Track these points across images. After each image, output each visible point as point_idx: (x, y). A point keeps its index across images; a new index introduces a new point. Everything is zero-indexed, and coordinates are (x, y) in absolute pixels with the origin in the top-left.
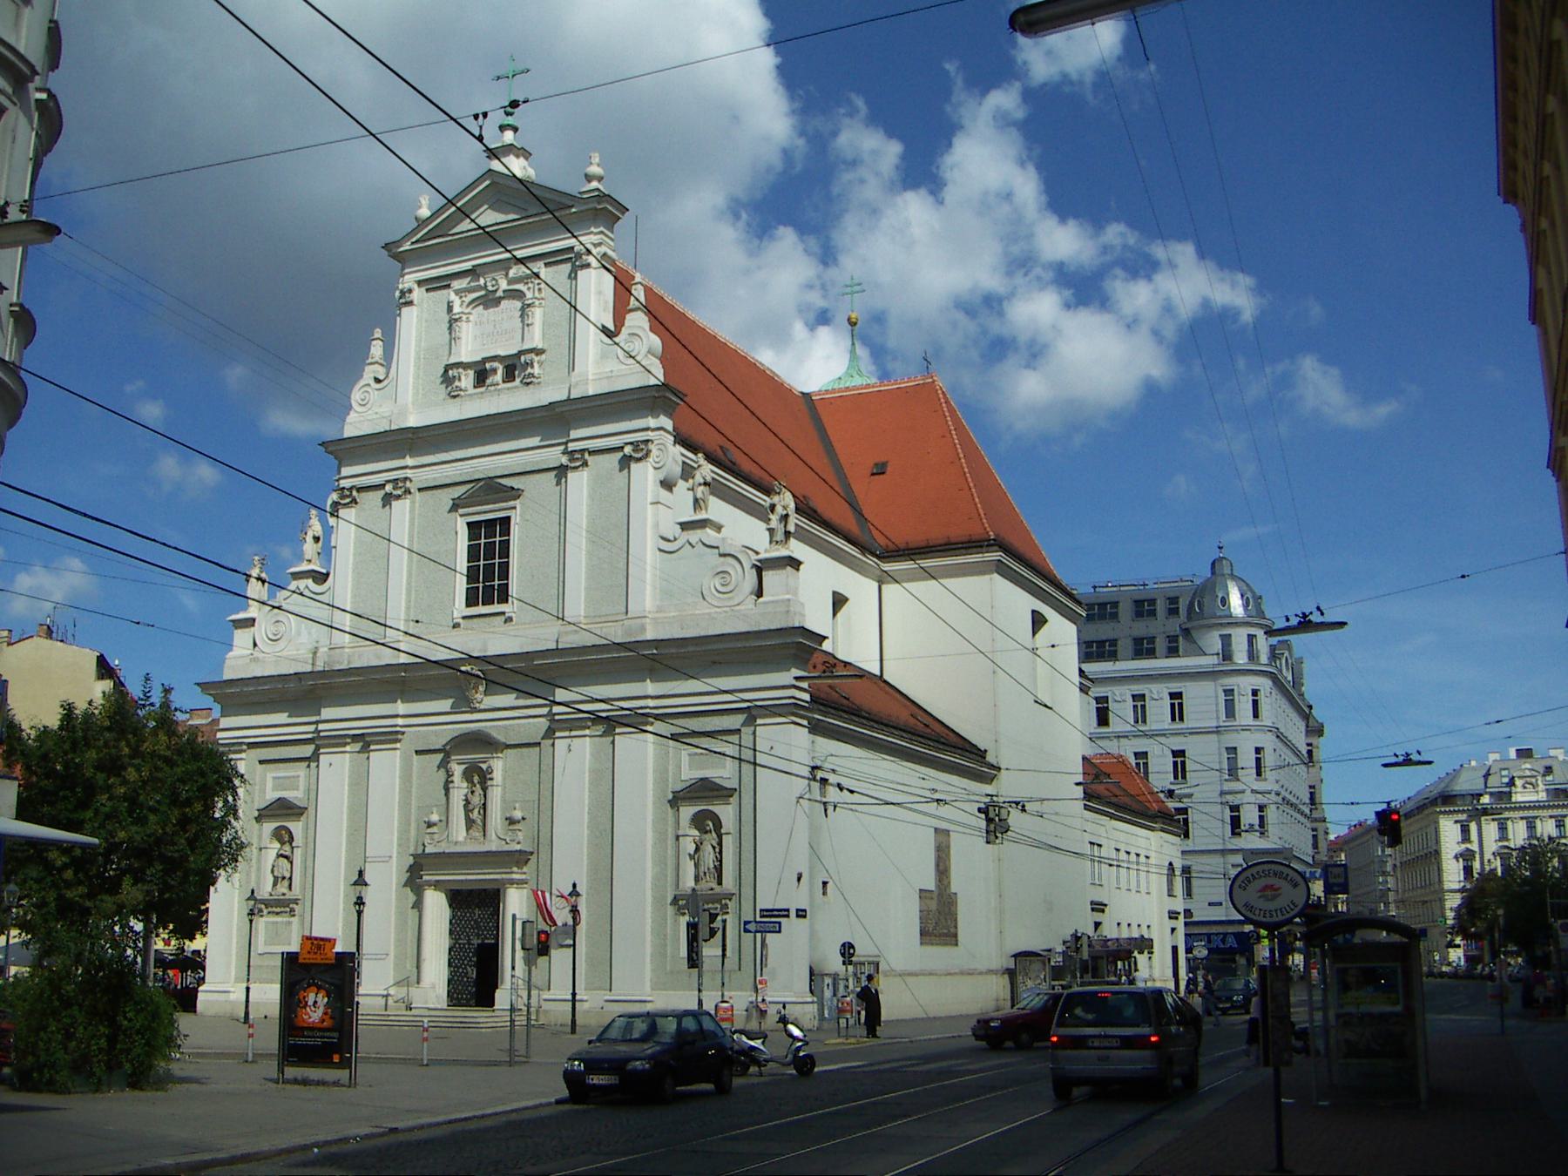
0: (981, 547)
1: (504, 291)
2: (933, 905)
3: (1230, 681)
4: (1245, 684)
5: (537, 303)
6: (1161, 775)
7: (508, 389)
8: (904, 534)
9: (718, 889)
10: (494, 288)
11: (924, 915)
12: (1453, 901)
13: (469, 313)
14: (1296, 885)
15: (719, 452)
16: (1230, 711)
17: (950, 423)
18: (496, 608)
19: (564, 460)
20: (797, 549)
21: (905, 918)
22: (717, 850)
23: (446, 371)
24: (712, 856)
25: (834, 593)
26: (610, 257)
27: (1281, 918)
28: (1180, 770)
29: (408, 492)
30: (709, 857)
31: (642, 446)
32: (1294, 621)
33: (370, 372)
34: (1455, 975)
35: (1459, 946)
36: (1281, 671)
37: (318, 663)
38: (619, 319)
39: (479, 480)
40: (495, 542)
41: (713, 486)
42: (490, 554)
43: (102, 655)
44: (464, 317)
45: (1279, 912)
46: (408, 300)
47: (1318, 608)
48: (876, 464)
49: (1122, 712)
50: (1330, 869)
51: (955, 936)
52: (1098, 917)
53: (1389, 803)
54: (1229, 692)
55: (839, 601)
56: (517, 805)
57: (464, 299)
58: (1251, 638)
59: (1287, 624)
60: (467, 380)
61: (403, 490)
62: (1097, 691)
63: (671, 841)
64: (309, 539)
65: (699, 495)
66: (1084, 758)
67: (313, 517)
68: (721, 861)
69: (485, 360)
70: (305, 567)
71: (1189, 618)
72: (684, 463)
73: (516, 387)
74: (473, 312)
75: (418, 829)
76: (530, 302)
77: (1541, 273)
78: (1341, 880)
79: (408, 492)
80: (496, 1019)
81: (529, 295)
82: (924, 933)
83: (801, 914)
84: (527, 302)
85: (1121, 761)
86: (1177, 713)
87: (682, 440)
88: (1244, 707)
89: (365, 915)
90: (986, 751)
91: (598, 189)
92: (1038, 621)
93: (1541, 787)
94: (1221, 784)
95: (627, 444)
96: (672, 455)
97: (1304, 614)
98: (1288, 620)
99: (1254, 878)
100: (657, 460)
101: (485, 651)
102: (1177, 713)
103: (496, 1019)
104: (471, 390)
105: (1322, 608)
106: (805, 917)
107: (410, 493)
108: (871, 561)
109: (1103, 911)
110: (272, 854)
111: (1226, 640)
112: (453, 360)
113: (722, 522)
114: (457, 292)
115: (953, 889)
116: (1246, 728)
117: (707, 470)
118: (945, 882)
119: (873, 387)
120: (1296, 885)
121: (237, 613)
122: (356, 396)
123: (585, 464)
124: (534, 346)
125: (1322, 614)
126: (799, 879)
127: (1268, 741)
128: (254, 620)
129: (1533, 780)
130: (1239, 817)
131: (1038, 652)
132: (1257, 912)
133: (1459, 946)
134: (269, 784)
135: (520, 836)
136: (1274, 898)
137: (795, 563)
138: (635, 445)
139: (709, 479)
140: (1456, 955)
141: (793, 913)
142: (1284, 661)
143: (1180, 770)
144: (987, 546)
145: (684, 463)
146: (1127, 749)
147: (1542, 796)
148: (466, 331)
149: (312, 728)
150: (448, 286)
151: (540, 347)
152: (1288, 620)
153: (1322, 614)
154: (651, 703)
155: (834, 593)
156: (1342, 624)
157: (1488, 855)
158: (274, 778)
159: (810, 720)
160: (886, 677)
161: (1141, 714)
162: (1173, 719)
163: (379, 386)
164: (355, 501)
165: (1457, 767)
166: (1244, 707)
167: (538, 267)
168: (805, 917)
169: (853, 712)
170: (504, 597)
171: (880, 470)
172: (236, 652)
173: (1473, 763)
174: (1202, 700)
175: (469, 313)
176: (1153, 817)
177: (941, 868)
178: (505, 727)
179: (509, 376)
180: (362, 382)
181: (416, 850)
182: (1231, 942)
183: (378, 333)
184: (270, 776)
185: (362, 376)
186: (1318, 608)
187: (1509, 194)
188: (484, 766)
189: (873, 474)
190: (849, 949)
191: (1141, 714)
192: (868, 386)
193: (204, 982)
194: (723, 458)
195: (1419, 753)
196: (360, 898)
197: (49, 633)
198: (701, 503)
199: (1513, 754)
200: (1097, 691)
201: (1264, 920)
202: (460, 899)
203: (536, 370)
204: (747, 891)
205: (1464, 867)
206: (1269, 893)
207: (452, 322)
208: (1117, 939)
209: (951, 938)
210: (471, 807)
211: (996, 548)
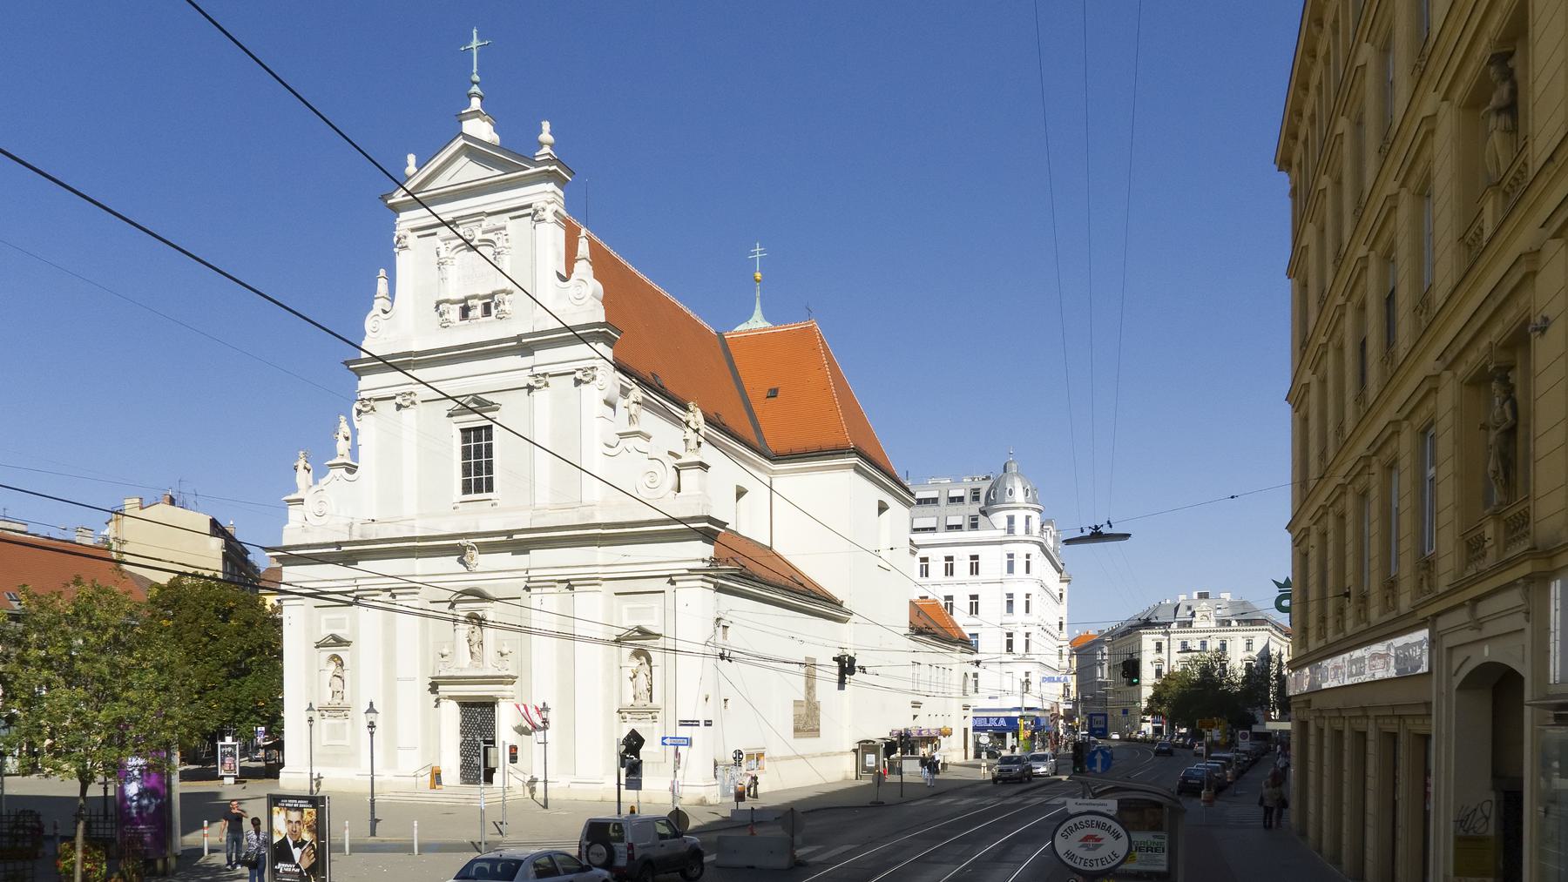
0: (844, 453)
1: (479, 241)
2: (803, 711)
3: (1011, 548)
4: (1020, 551)
5: (505, 251)
6: (961, 617)
7: (486, 322)
8: (783, 448)
9: (649, 705)
10: (471, 238)
11: (797, 718)
12: (1147, 692)
13: (453, 258)
14: (1118, 837)
15: (651, 377)
16: (1011, 569)
17: (824, 359)
18: (485, 495)
19: (532, 382)
20: (708, 454)
21: (785, 720)
22: (649, 677)
23: (437, 307)
24: (645, 682)
25: (737, 486)
26: (559, 214)
27: (1101, 867)
28: (974, 609)
29: (413, 403)
30: (642, 681)
31: (589, 372)
32: (1087, 532)
33: (379, 304)
34: (1144, 740)
35: (1149, 721)
36: (1046, 540)
37: (354, 534)
38: (570, 269)
39: (468, 396)
40: (474, 442)
41: (644, 404)
42: (478, 455)
43: (214, 519)
44: (449, 261)
45: (1099, 862)
46: (404, 245)
47: (1109, 522)
48: (770, 390)
49: (936, 568)
50: (1094, 717)
51: (818, 730)
52: (916, 711)
53: (1131, 655)
54: (1011, 556)
55: (741, 493)
56: (505, 643)
57: (448, 246)
58: (1028, 518)
59: (1082, 535)
60: (454, 312)
61: (409, 401)
62: (922, 553)
63: (616, 670)
64: (341, 437)
65: (632, 412)
66: (911, 602)
67: (342, 421)
68: (651, 685)
69: (466, 299)
70: (338, 460)
71: (986, 504)
72: (621, 385)
73: (491, 321)
74: (457, 256)
75: (434, 658)
76: (500, 250)
77: (1310, 231)
78: (1103, 726)
79: (413, 403)
80: (492, 796)
81: (499, 244)
82: (796, 730)
83: (708, 723)
84: (497, 250)
85: (935, 604)
86: (974, 569)
87: (620, 367)
88: (1020, 565)
89: (374, 737)
90: (842, 602)
91: (549, 154)
92: (882, 508)
93: (1213, 618)
94: (1001, 618)
95: (578, 370)
96: (609, 379)
97: (1096, 526)
98: (1082, 531)
99: (1077, 828)
100: (601, 383)
101: (478, 528)
102: (974, 569)
103: (492, 796)
104: (458, 322)
105: (1111, 522)
106: (711, 725)
107: (415, 404)
108: (766, 463)
109: (919, 707)
110: (330, 674)
111: (1011, 520)
112: (442, 297)
113: (651, 434)
114: (444, 240)
115: (818, 699)
116: (1021, 580)
117: (637, 393)
118: (812, 694)
119: (769, 330)
120: (1118, 837)
121: (290, 495)
122: (369, 324)
123: (547, 385)
124: (504, 288)
125: (1111, 526)
126: (706, 699)
127: (1035, 589)
128: (303, 500)
129: (1208, 614)
130: (1012, 640)
131: (880, 554)
132: (1078, 861)
133: (1149, 721)
134: (323, 626)
135: (508, 665)
136: (1095, 848)
137: (703, 466)
138: (584, 370)
139: (640, 400)
140: (1148, 727)
141: (702, 723)
142: (1048, 533)
143: (974, 609)
144: (849, 453)
145: (621, 385)
146: (938, 595)
147: (1213, 624)
148: (452, 271)
149: (352, 582)
150: (435, 234)
151: (508, 289)
152: (1082, 531)
153: (1111, 526)
154: (599, 570)
155: (737, 486)
156: (1126, 536)
157: (1173, 662)
158: (327, 620)
159: (715, 584)
160: (775, 548)
161: (949, 571)
162: (972, 573)
163: (386, 316)
164: (373, 409)
165: (1157, 604)
166: (1020, 565)
167: (503, 220)
168: (711, 725)
169: (745, 576)
170: (490, 489)
171: (773, 393)
172: (291, 524)
173: (1168, 602)
174: (991, 560)
175: (453, 258)
176: (955, 643)
177: (809, 685)
178: (494, 585)
179: (487, 310)
180: (372, 313)
181: (434, 673)
182: (1003, 723)
183: (382, 272)
184: (324, 617)
185: (372, 309)
186: (1109, 522)
187: (1285, 163)
188: (480, 614)
189: (768, 397)
190: (739, 754)
191: (949, 571)
192: (765, 329)
193: (284, 766)
194: (654, 383)
195: (1157, 618)
196: (372, 723)
197: (172, 502)
198: (635, 419)
199: (1195, 596)
200: (922, 553)
201: (1084, 868)
202: (466, 705)
203: (506, 307)
204: (670, 707)
205: (1156, 670)
206: (1091, 842)
207: (441, 264)
208: (929, 730)
209: (814, 731)
210: (472, 643)
211: (854, 454)
